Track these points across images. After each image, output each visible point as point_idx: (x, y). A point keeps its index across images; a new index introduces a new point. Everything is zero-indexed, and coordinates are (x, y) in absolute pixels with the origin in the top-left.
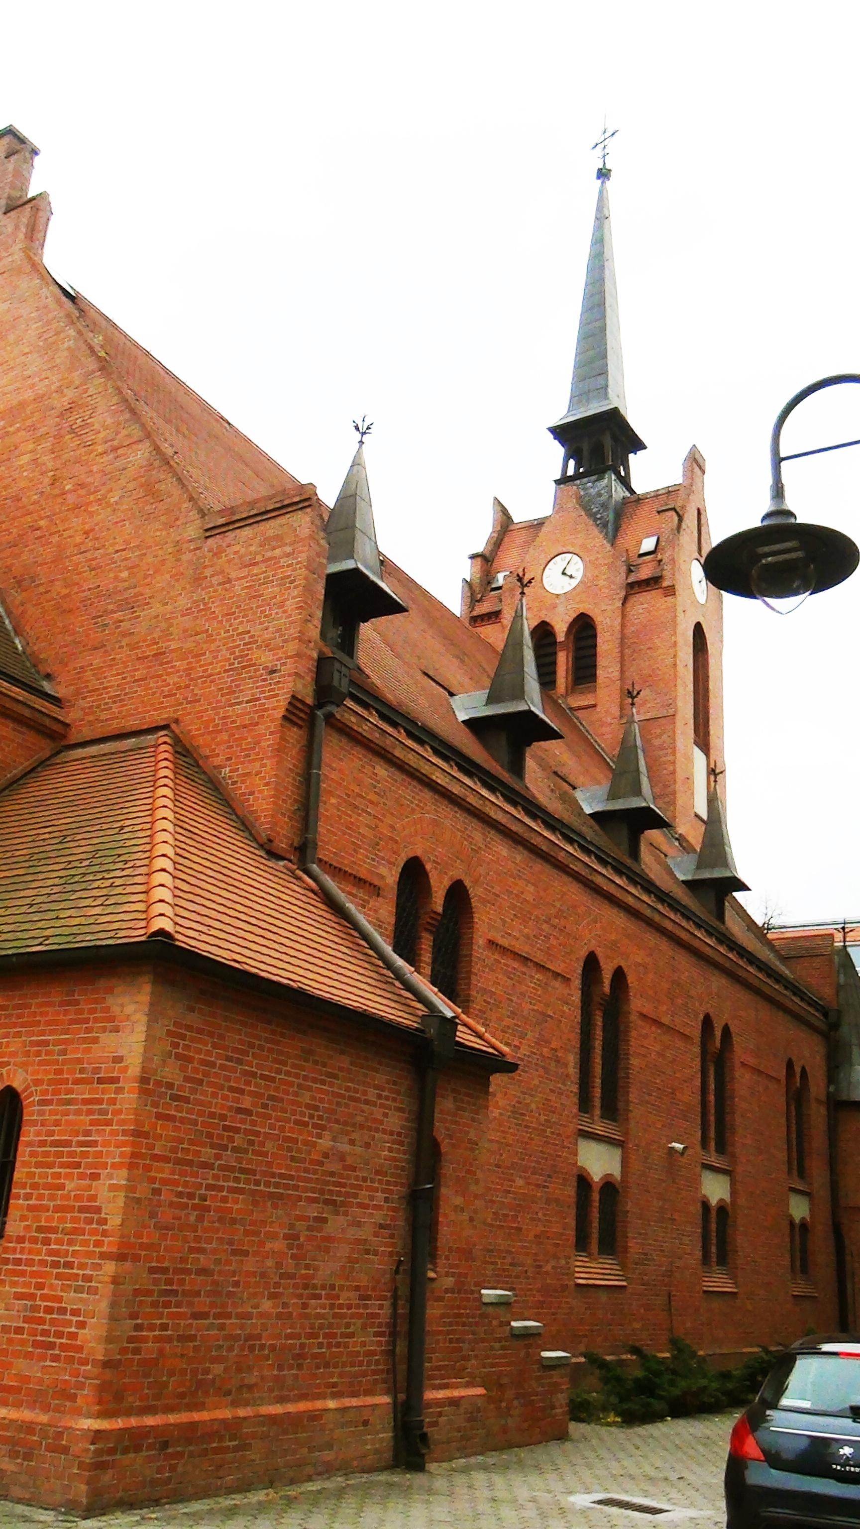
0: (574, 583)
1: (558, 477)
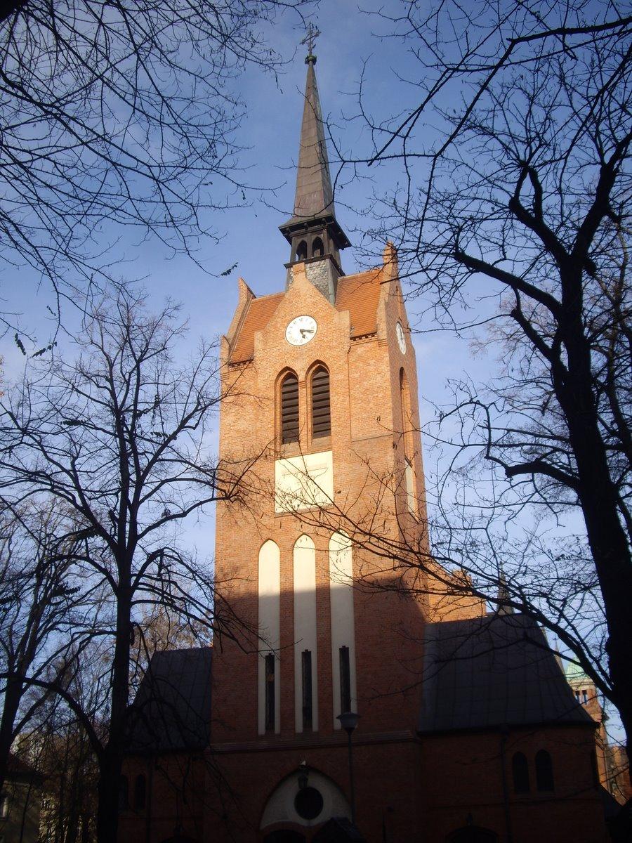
0: (305, 341)
1: (288, 261)
